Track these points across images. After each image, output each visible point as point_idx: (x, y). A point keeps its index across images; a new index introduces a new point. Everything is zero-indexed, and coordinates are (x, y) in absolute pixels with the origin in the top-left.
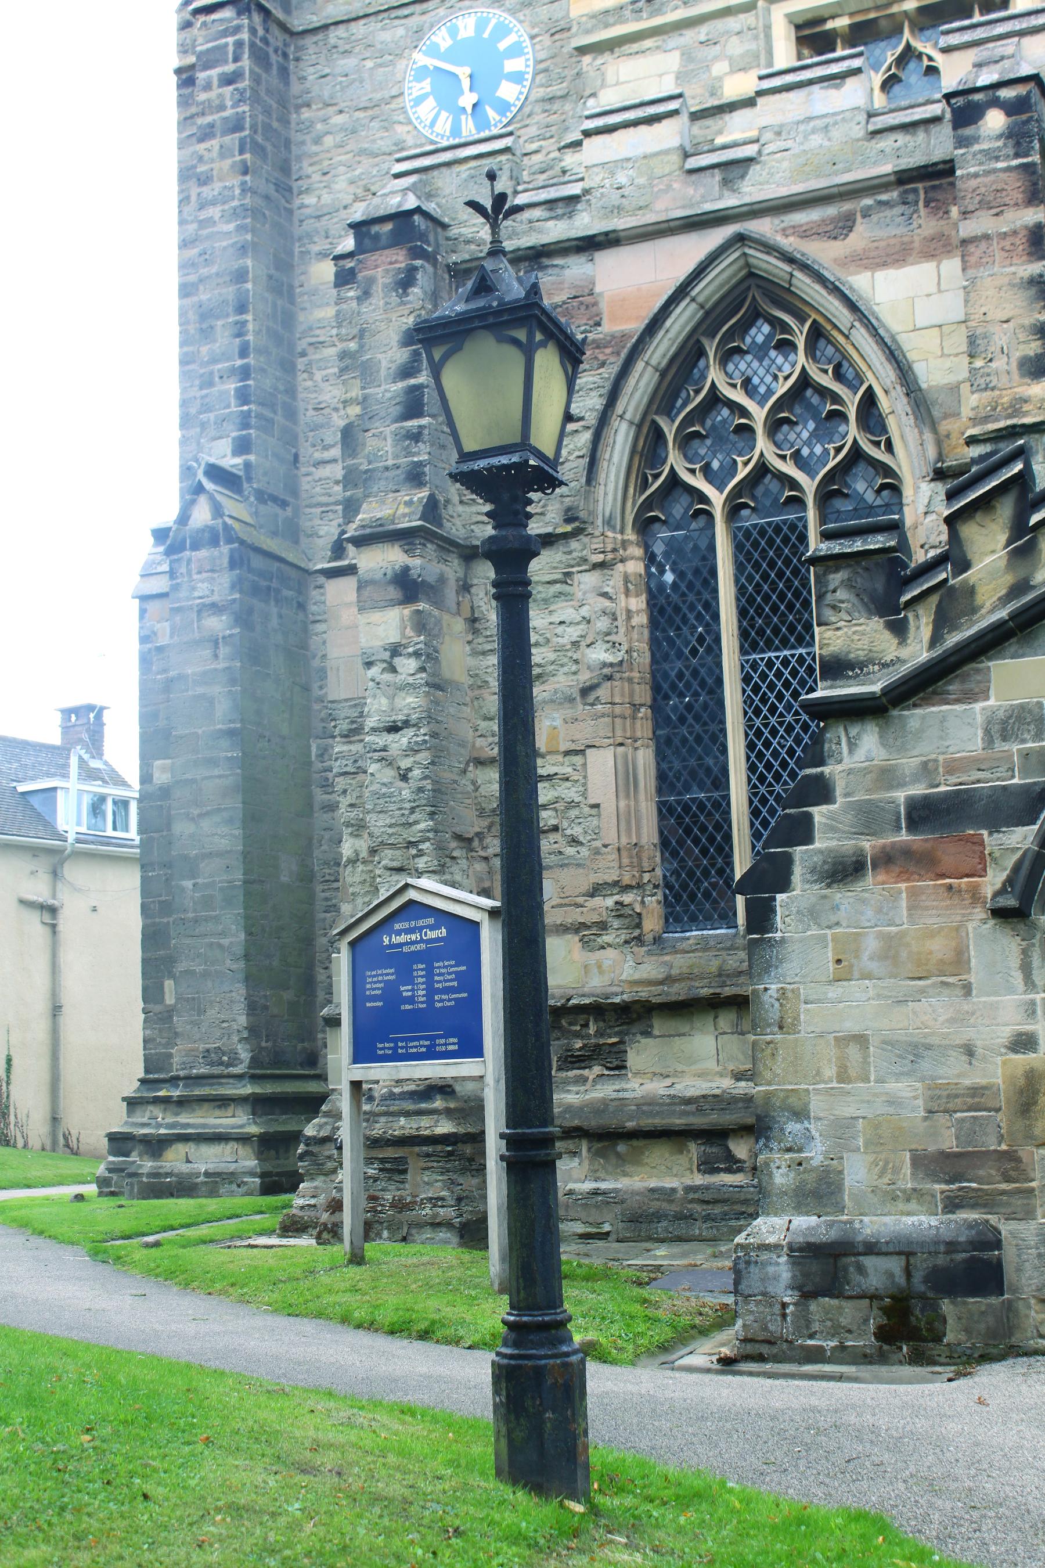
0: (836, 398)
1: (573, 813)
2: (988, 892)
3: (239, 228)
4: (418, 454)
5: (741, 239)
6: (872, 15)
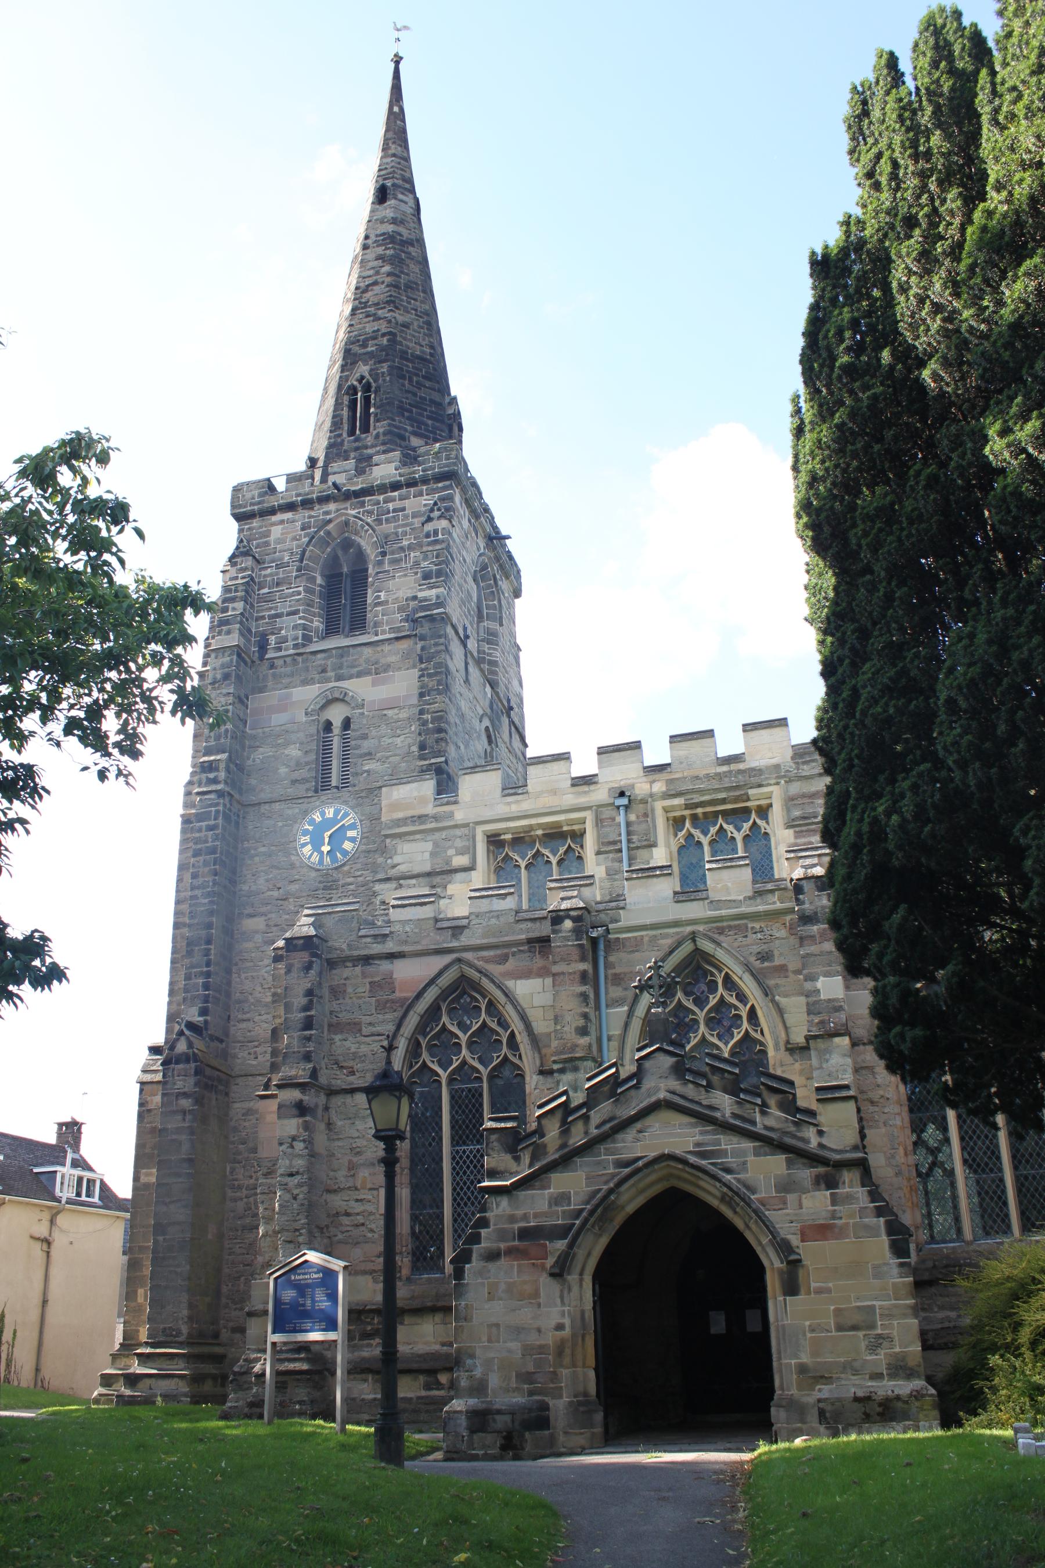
1: (372, 1218)
2: (548, 1266)
3: (211, 902)
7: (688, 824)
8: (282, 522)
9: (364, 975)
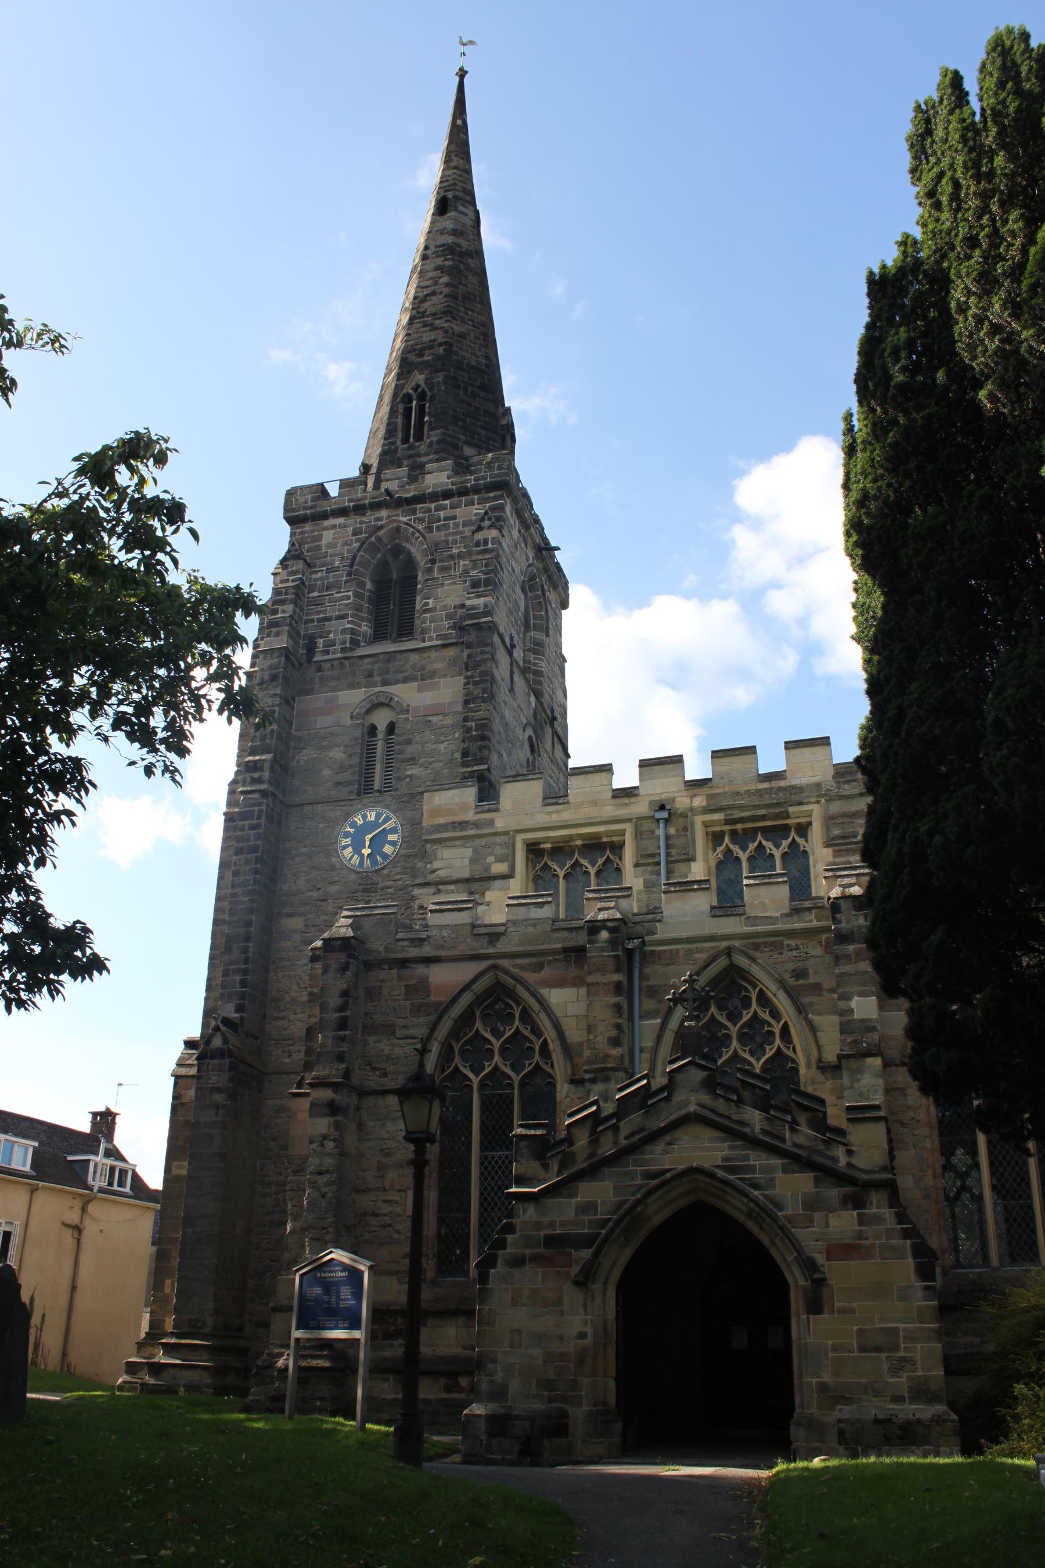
0: (531, 1042)
1: (399, 1219)
2: (573, 1274)
4: (343, 1047)
5: (495, 967)
6: (561, 845)
7: (727, 840)
9: (400, 978)
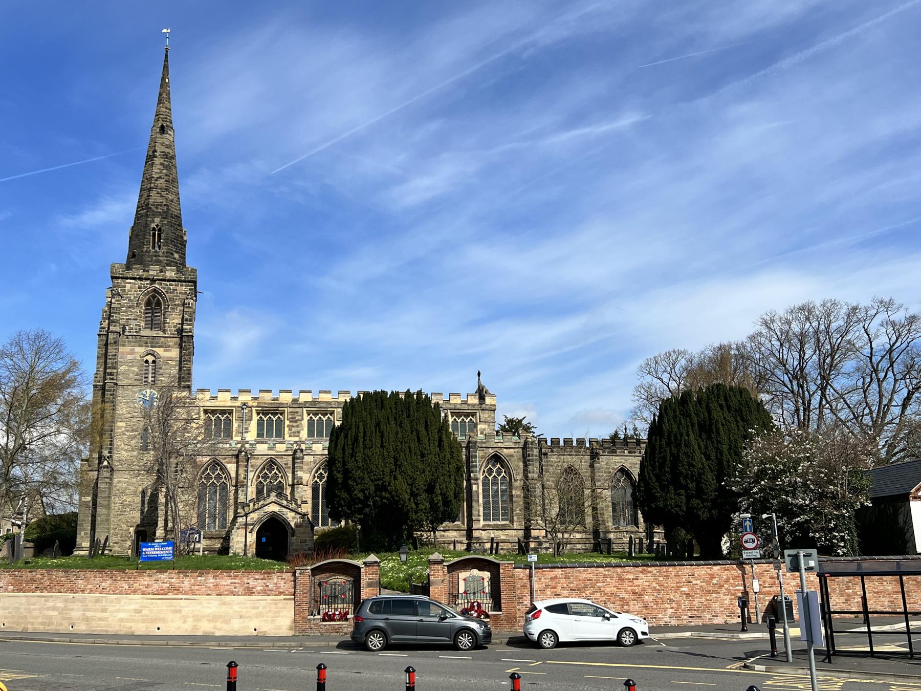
8: (130, 283)
